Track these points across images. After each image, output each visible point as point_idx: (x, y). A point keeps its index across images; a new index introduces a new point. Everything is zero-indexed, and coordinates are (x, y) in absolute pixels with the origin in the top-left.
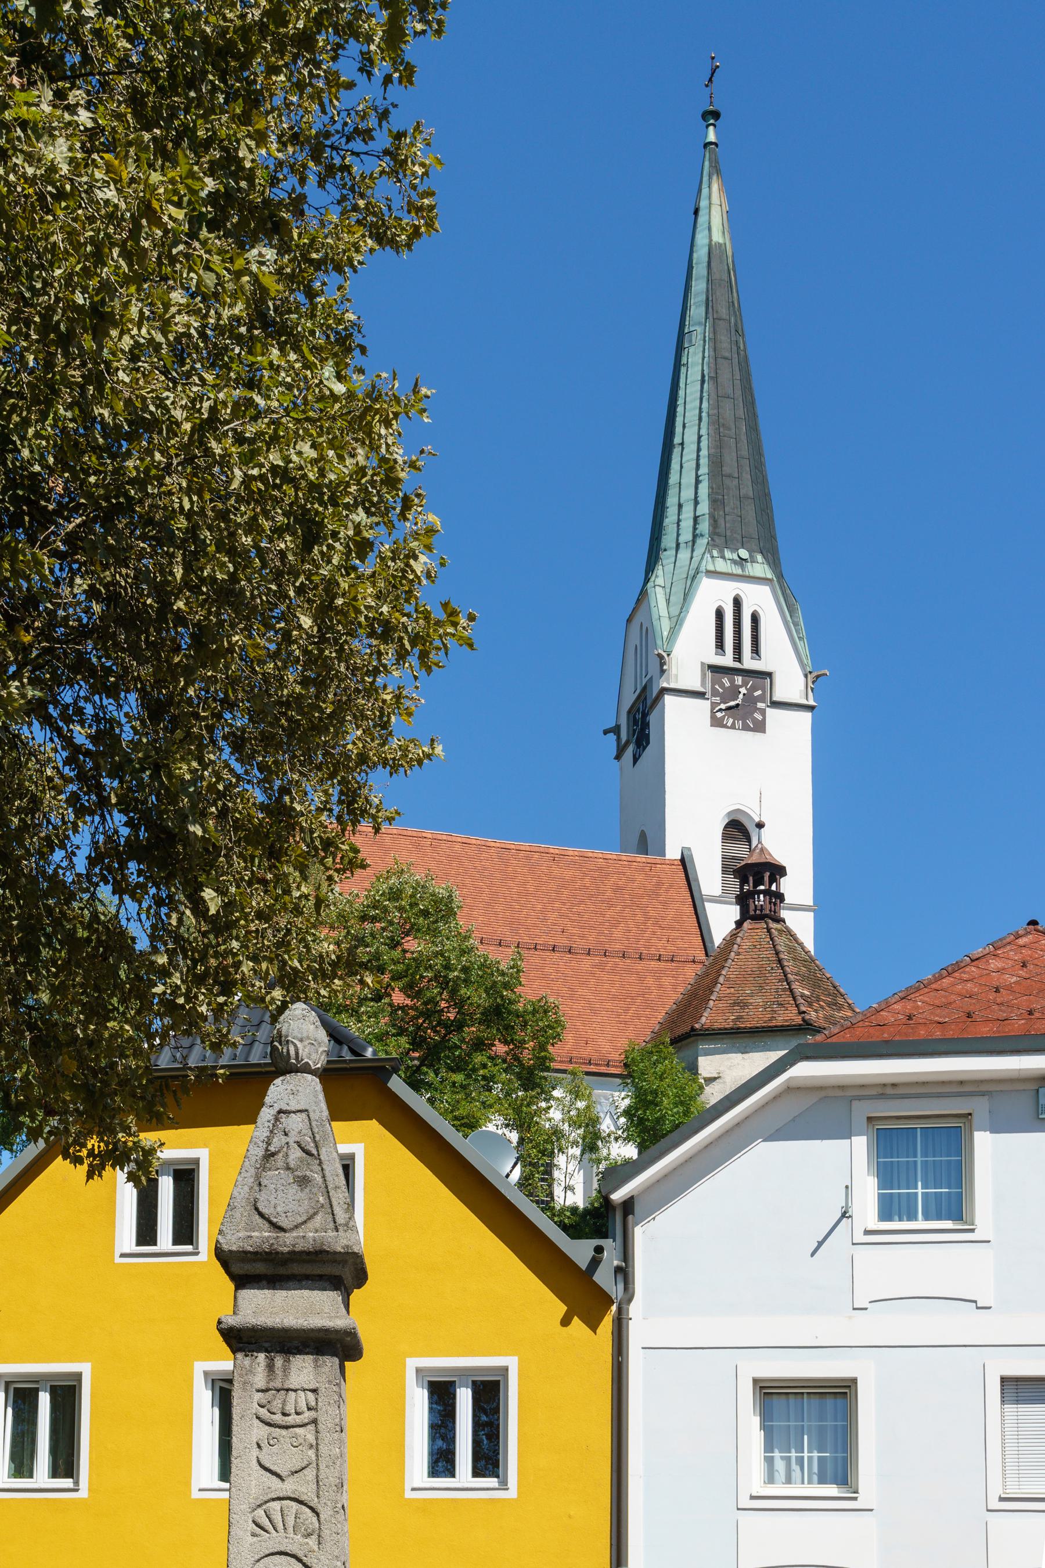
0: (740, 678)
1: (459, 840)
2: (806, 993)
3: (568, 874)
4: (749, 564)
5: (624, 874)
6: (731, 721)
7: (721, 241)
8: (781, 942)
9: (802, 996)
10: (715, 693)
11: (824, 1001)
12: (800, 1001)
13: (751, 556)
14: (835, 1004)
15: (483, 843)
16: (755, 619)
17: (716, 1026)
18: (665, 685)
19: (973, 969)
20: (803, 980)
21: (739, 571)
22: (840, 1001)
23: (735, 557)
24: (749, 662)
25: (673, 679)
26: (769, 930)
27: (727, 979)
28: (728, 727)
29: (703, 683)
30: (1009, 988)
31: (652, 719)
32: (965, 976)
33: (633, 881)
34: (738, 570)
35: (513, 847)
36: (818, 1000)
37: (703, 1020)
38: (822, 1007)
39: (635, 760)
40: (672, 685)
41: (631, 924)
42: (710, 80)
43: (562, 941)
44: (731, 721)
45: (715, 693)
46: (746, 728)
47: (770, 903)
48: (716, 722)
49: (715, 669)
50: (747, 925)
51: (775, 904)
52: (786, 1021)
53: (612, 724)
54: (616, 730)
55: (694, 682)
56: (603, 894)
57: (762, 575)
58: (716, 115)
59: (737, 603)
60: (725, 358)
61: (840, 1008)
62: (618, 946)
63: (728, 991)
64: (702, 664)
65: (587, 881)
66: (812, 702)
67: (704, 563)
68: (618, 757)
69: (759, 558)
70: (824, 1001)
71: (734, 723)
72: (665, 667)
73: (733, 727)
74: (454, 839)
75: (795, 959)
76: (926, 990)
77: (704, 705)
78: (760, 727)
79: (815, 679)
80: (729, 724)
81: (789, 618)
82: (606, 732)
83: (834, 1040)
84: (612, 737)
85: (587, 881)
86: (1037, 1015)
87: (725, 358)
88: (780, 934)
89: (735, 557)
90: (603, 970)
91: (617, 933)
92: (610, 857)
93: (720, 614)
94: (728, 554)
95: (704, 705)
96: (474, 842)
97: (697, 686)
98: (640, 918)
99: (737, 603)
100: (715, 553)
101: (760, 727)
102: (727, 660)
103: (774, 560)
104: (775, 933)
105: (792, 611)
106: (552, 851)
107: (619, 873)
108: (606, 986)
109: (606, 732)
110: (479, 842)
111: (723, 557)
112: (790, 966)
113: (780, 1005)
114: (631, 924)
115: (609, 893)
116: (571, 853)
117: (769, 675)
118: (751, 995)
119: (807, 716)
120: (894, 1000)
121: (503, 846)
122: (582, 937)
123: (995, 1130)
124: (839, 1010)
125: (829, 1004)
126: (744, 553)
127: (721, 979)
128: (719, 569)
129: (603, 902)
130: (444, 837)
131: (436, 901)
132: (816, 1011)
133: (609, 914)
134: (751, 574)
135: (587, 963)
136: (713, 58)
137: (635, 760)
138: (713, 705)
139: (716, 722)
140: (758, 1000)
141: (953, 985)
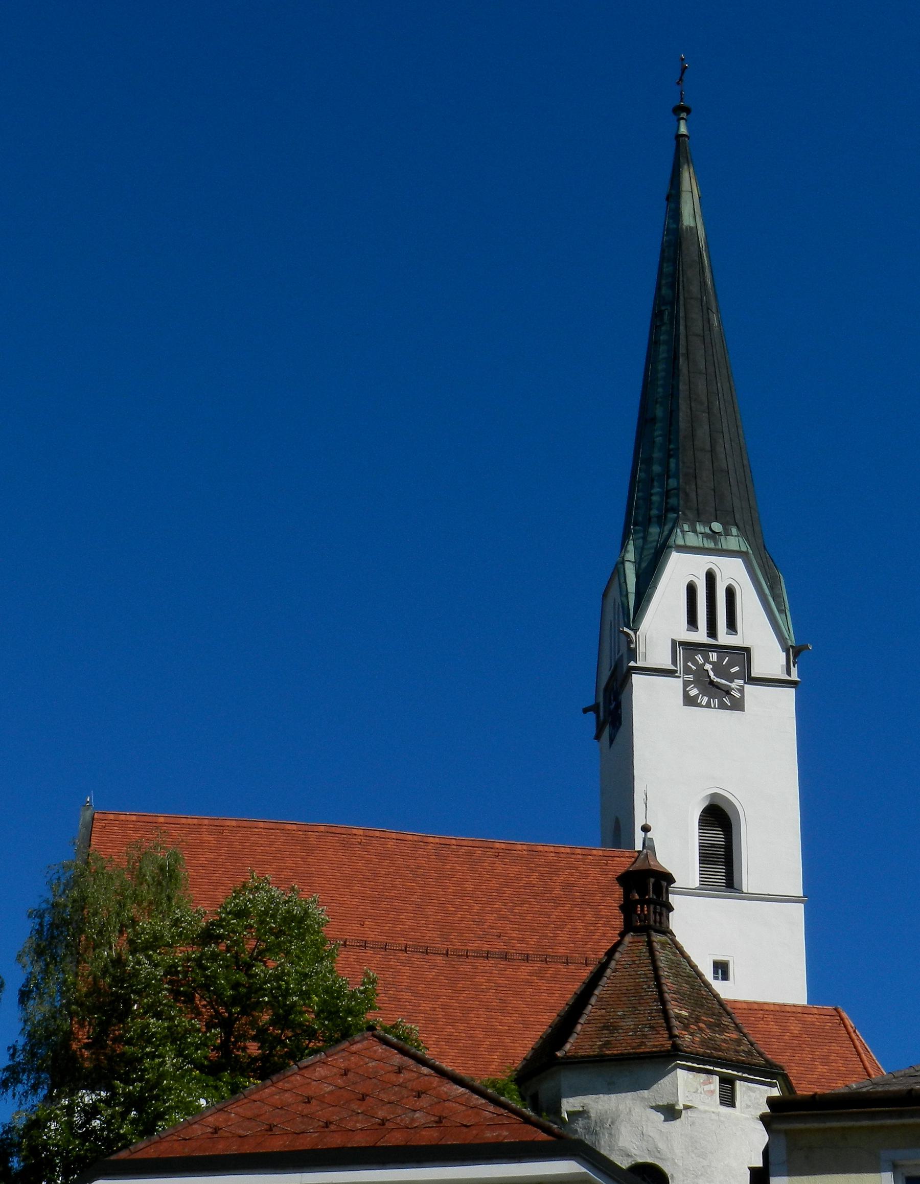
0: (715, 654)
1: (394, 836)
2: (684, 1013)
3: (513, 870)
4: (722, 537)
5: (576, 868)
6: (706, 699)
7: (692, 224)
8: (663, 957)
9: (678, 1017)
10: (687, 671)
11: (704, 1022)
12: (675, 1022)
13: (724, 528)
14: (718, 1026)
15: (420, 839)
16: (730, 593)
17: (581, 1053)
18: (632, 664)
19: (298, 1078)
20: (682, 1000)
21: (712, 545)
22: (726, 1021)
23: (707, 530)
24: (724, 638)
25: (640, 656)
26: (650, 943)
27: (600, 999)
28: (702, 706)
29: (674, 661)
30: (321, 1099)
31: (623, 697)
32: (287, 1086)
33: (587, 876)
34: (710, 544)
35: (454, 842)
36: (698, 1020)
37: (568, 1046)
38: (700, 1029)
39: (612, 740)
40: (640, 664)
41: (579, 925)
42: (681, 79)
43: (499, 946)
44: (706, 699)
45: (687, 671)
46: (722, 706)
47: (655, 913)
48: (690, 701)
49: (686, 645)
50: (628, 939)
51: (661, 914)
52: (656, 1046)
53: (591, 702)
54: (595, 708)
55: (665, 662)
56: (551, 892)
57: (736, 548)
58: (687, 110)
59: (711, 578)
60: (697, 335)
61: (723, 1029)
62: (561, 950)
63: (599, 1013)
64: (674, 642)
65: (534, 878)
66: (794, 677)
67: (673, 537)
68: (598, 737)
69: (734, 531)
70: (704, 1022)
71: (709, 701)
72: (632, 646)
73: (708, 705)
74: (387, 835)
75: (676, 975)
76: (246, 1101)
77: (676, 684)
78: (738, 705)
79: (794, 653)
80: (704, 703)
81: (767, 591)
82: (585, 711)
83: (138, 1156)
84: (591, 715)
85: (534, 878)
86: (332, 1127)
87: (697, 335)
88: (663, 948)
89: (707, 530)
90: (542, 978)
91: (563, 936)
92: (562, 850)
93: (691, 590)
94: (700, 528)
95: (676, 684)
96: (410, 838)
97: (667, 664)
98: (589, 917)
99: (711, 578)
100: (686, 528)
101: (738, 705)
102: (701, 636)
103: (750, 532)
104: (657, 946)
105: (773, 585)
106: (497, 845)
107: (570, 868)
108: (544, 996)
109: (585, 711)
110: (416, 838)
111: (694, 531)
112: (668, 983)
113: (652, 1028)
114: (579, 925)
115: (558, 891)
116: (519, 847)
117: (747, 650)
118: (622, 1017)
119: (791, 692)
120: (209, 1113)
121: (443, 841)
122: (521, 941)
123: (791, 1173)
124: (721, 1032)
125: (710, 1026)
126: (717, 527)
127: (593, 1000)
128: (688, 544)
129: (548, 901)
130: (377, 834)
131: (289, 918)
132: (692, 1034)
133: (556, 913)
134: (725, 547)
135: (524, 970)
136: (683, 59)
137: (612, 740)
138: (686, 684)
139: (690, 701)
140: (629, 1023)
141: (272, 1095)
